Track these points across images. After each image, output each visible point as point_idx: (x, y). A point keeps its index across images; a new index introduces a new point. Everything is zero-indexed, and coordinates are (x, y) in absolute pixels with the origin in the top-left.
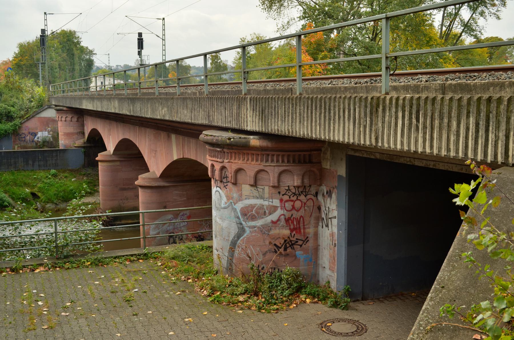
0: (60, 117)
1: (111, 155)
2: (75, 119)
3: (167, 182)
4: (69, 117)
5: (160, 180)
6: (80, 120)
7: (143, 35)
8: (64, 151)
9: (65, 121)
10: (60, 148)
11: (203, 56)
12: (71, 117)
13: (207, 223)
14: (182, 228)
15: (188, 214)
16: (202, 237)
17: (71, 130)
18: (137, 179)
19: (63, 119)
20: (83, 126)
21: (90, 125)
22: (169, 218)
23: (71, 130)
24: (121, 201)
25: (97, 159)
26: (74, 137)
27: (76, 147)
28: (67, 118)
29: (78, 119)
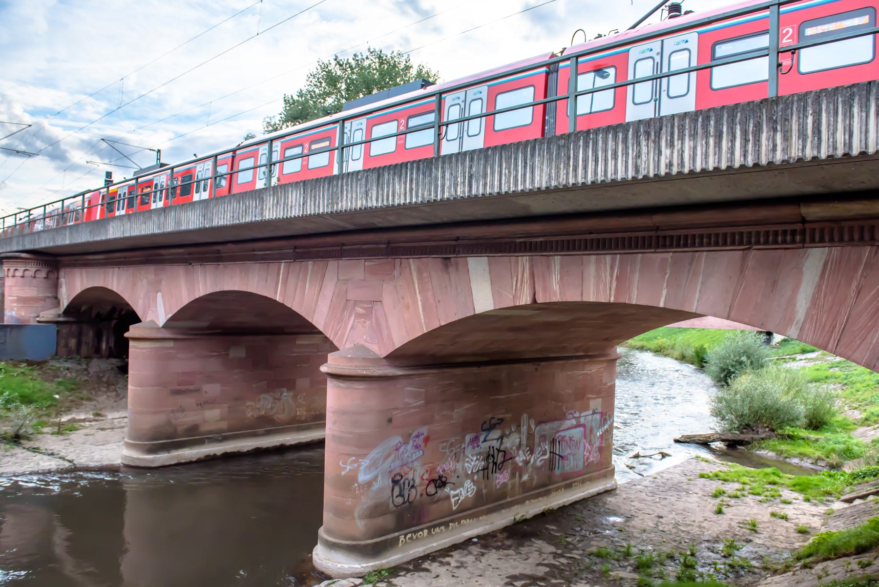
0: (12, 269)
1: (159, 329)
2: (42, 274)
3: (397, 367)
4: (32, 269)
5: (384, 362)
6: (52, 276)
8: (18, 327)
10: (5, 323)
12: (34, 269)
13: (452, 451)
14: (416, 463)
15: (426, 434)
16: (444, 479)
17: (32, 292)
18: (325, 361)
19: (19, 273)
20: (56, 286)
23: (32, 292)
24: (172, 415)
25: (126, 335)
27: (39, 322)
28: (26, 272)
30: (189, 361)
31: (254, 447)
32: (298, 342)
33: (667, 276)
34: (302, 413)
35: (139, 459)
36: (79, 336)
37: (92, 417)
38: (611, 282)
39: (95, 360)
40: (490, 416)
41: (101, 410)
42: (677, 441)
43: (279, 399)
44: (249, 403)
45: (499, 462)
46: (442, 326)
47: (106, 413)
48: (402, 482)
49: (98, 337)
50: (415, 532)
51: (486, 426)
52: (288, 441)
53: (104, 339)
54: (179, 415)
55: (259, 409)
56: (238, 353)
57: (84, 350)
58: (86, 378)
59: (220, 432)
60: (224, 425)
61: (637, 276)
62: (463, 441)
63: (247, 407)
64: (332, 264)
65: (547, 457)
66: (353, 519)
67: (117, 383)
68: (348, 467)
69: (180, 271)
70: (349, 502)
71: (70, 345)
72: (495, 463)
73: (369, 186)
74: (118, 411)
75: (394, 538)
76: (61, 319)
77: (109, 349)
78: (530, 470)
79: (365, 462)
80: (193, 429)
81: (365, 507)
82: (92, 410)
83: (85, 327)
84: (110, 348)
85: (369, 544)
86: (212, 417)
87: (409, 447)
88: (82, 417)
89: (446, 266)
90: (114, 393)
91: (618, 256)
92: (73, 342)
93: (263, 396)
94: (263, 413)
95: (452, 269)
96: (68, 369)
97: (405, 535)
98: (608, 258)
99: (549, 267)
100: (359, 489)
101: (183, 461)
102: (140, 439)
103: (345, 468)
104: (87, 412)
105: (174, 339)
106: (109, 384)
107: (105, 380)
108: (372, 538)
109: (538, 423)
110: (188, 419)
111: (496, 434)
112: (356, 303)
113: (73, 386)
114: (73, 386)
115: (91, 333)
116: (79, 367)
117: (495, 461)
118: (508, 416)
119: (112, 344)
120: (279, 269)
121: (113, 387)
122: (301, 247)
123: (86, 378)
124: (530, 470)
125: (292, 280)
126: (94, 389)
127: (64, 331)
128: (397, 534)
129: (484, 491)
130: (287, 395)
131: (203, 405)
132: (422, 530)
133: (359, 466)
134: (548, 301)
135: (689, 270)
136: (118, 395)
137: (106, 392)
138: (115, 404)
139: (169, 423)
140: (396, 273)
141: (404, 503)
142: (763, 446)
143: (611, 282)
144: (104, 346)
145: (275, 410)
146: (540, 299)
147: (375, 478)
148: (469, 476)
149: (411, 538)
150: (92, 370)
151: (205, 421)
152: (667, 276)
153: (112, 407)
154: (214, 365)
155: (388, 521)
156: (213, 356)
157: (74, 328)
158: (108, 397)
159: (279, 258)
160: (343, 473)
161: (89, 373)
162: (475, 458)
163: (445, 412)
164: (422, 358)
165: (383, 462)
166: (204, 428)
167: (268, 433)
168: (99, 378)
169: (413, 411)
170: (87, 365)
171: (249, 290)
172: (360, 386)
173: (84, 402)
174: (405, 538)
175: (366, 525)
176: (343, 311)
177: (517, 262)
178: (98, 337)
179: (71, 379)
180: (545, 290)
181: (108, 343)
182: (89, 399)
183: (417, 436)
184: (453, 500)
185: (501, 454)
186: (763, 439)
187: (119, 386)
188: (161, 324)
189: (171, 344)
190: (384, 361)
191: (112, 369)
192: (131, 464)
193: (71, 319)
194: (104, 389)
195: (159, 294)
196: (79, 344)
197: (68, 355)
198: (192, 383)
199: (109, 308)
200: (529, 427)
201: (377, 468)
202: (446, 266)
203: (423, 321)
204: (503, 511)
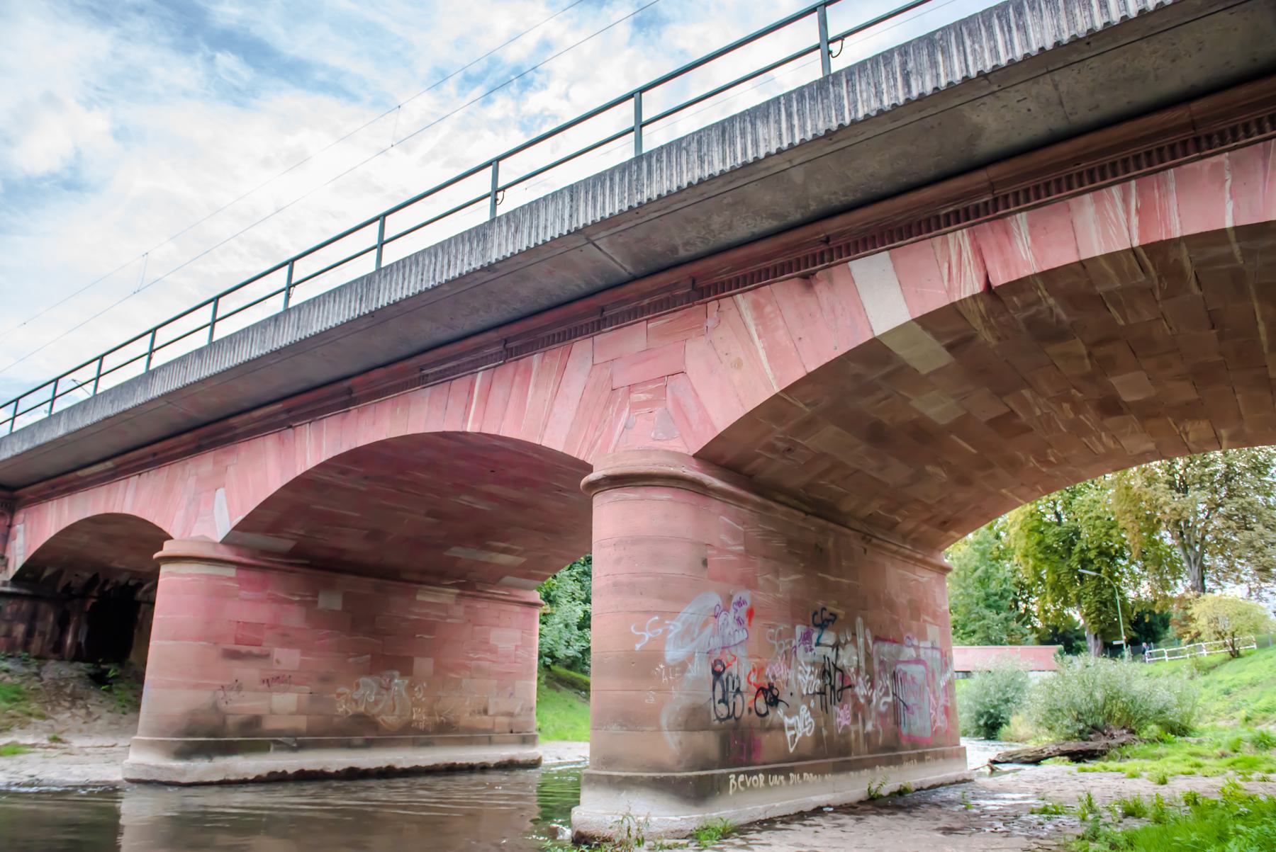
1: (215, 544)
5: (694, 463)
24: (221, 694)
30: (251, 607)
31: (346, 766)
32: (419, 597)
33: (1228, 184)
34: (420, 717)
35: (158, 768)
36: (32, 621)
37: (46, 742)
38: (1128, 220)
39: (52, 662)
40: (820, 604)
41: (62, 732)
42: (971, 781)
43: (388, 689)
44: (341, 690)
45: (837, 688)
46: (809, 375)
47: (69, 739)
48: (724, 676)
49: (62, 624)
50: (750, 774)
51: (818, 620)
52: (399, 761)
53: (71, 629)
54: (233, 695)
55: (356, 701)
56: (331, 601)
57: (36, 644)
58: (38, 685)
59: (295, 734)
60: (301, 723)
61: (1173, 200)
62: (792, 635)
63: (339, 695)
64: (581, 347)
65: (890, 699)
66: (659, 729)
67: (89, 697)
68: (647, 635)
69: (269, 443)
70: (651, 699)
71: (15, 634)
72: (833, 688)
73: (705, 149)
74: (90, 737)
75: (722, 775)
76: (8, 589)
77: (77, 645)
78: (873, 714)
79: (676, 627)
80: (252, 724)
81: (678, 708)
82: (46, 732)
83: (43, 606)
84: (79, 644)
85: (689, 778)
86: (283, 707)
87: (731, 617)
88: (30, 741)
89: (809, 287)
90: (83, 711)
91: (1133, 183)
92: (20, 630)
93: (364, 680)
94: (362, 709)
95: (820, 288)
96: (7, 671)
97: (737, 774)
98: (1115, 190)
99: (1007, 232)
100: (667, 674)
101: (232, 778)
102: (163, 733)
103: (642, 636)
104: (37, 735)
105: (239, 565)
106: (75, 698)
107: (68, 690)
108: (691, 769)
109: (877, 639)
110: (244, 704)
111: (829, 637)
112: (631, 388)
113: (15, 696)
114: (15, 696)
115: (51, 618)
116: (26, 671)
117: (834, 684)
118: (841, 613)
119: (82, 640)
120: (472, 385)
121: (80, 702)
122: (517, 337)
123: (38, 685)
124: (873, 714)
125: (498, 392)
126: (51, 701)
127: (8, 609)
128: (724, 771)
129: (825, 733)
130: (399, 683)
131: (274, 681)
132: (756, 773)
133: (666, 632)
134: (1015, 278)
135: (1265, 166)
136: (89, 714)
137: (69, 709)
138: (84, 727)
139: (215, 707)
140: (710, 323)
141: (729, 717)
142: (1128, 753)
143: (1128, 220)
144: (69, 640)
145: (381, 706)
146: (998, 279)
147: (691, 658)
148: (805, 698)
149: (744, 784)
150: (47, 676)
151: (272, 712)
152: (1228, 184)
153: (80, 731)
154: (294, 618)
155: (708, 742)
156: (291, 602)
157: (25, 606)
158: (73, 716)
159: (472, 368)
160: (638, 646)
161: (42, 680)
162: (809, 669)
163: (768, 576)
164: (739, 466)
165: (701, 632)
166: (270, 724)
167: (369, 744)
168: (59, 688)
169: (731, 557)
170: (39, 667)
171: (409, 432)
172: (662, 496)
173: (33, 720)
174: (736, 780)
175: (680, 743)
176: (606, 407)
177: (947, 242)
178: (62, 624)
179: (12, 685)
180: (1006, 264)
181: (75, 636)
182: (42, 717)
183: (740, 603)
184: (789, 734)
185: (838, 674)
186: (1123, 744)
187: (90, 701)
188: (219, 538)
189: (231, 572)
190: (694, 461)
191: (80, 677)
192: (145, 777)
193: (24, 591)
194: (67, 704)
195: (221, 492)
196: (29, 633)
197: (8, 650)
198: (257, 644)
199: (87, 575)
200: (866, 643)
201: (693, 640)
202: (809, 287)
203: (771, 377)
204: (852, 773)
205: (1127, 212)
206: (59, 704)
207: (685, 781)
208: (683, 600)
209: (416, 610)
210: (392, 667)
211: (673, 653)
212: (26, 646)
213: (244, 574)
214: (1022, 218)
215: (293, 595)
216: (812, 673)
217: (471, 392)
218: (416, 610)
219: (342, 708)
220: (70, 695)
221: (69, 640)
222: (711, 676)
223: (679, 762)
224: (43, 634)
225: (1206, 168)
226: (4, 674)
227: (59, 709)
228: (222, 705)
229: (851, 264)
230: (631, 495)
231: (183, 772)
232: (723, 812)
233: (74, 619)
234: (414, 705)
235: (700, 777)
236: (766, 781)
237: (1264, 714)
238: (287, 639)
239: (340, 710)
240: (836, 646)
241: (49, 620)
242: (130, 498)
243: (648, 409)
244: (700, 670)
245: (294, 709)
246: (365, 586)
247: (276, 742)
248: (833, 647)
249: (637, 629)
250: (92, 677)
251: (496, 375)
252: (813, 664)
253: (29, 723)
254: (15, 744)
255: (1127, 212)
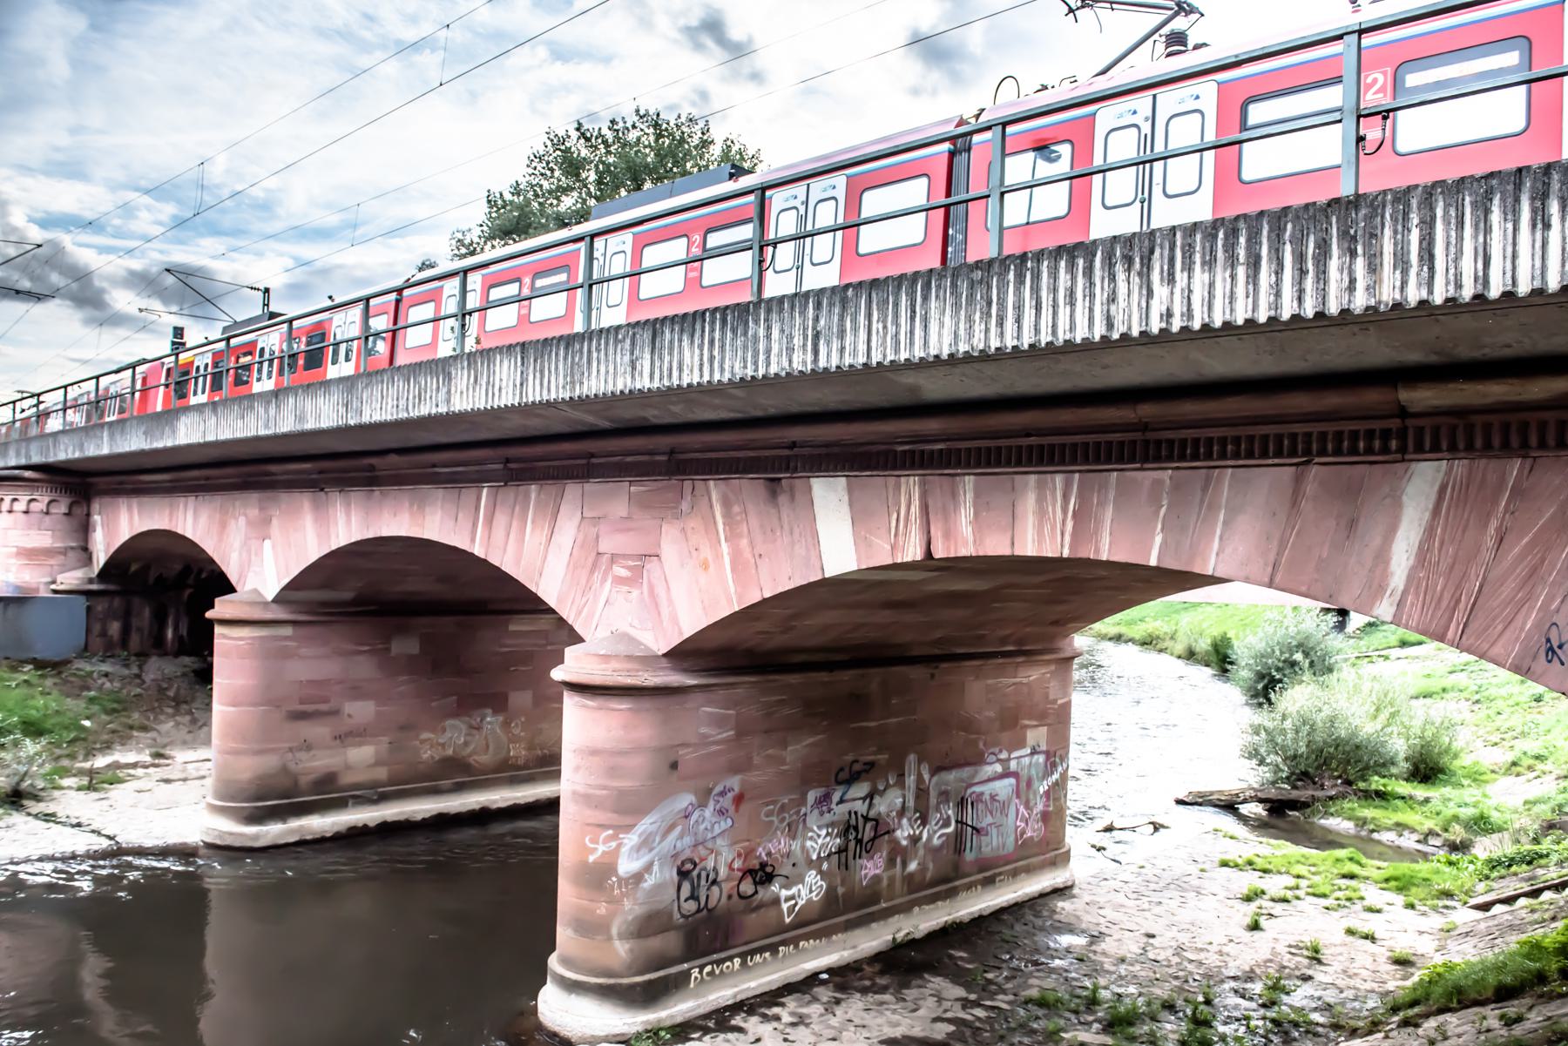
2: (61, 508)
3: (685, 671)
5: (665, 663)
6: (78, 511)
7: (186, 333)
9: (26, 512)
11: (642, 296)
12: (47, 499)
13: (783, 820)
14: (719, 842)
15: (737, 790)
16: (769, 869)
21: (119, 525)
22: (685, 804)
25: (209, 614)
26: (52, 562)
27: (55, 592)
29: (70, 507)
30: (316, 662)
32: (512, 628)
33: (1163, 510)
34: (518, 752)
35: (231, 834)
36: (126, 618)
37: (148, 759)
40: (849, 758)
41: (165, 746)
43: (479, 728)
44: (425, 735)
45: (866, 839)
46: (765, 601)
47: (172, 753)
49: (160, 619)
51: (843, 775)
52: (495, 801)
53: (170, 622)
54: (303, 755)
55: (443, 745)
57: (135, 641)
59: (373, 785)
60: (382, 773)
62: (803, 801)
63: (423, 742)
66: (610, 938)
67: (194, 699)
68: (601, 848)
69: (304, 502)
70: (602, 909)
72: (859, 841)
73: (637, 352)
74: (195, 749)
75: (681, 973)
76: (94, 587)
77: (178, 638)
78: (921, 852)
79: (631, 839)
80: (327, 781)
82: (149, 747)
83: (136, 601)
86: (361, 759)
87: (708, 812)
90: (188, 718)
92: (115, 628)
93: (449, 722)
94: (450, 752)
96: (106, 675)
97: (702, 968)
99: (954, 495)
100: (620, 887)
102: (233, 799)
104: (140, 751)
105: (294, 623)
107: (171, 693)
109: (935, 771)
111: (860, 789)
112: (614, 558)
113: (115, 706)
114: (115, 706)
115: (147, 612)
116: (126, 672)
118: (882, 758)
119: (184, 631)
120: (479, 499)
121: (185, 707)
124: (921, 852)
125: (501, 519)
129: (840, 890)
130: (491, 720)
133: (619, 846)
136: (194, 721)
137: (174, 716)
138: (189, 737)
139: (284, 770)
140: (685, 506)
141: (699, 910)
144: (170, 634)
145: (472, 747)
146: (939, 552)
147: (648, 868)
148: (815, 864)
149: (711, 974)
150: (149, 677)
151: (348, 767)
152: (1163, 510)
154: (364, 668)
155: (670, 942)
157: (117, 602)
158: (178, 724)
159: (478, 479)
162: (824, 832)
166: (347, 779)
167: (459, 788)
168: (162, 690)
170: (140, 667)
174: (701, 972)
176: (592, 571)
178: (160, 619)
180: (947, 535)
181: (176, 629)
182: (144, 729)
184: (785, 906)
186: (1331, 798)
187: (195, 705)
189: (288, 631)
191: (184, 675)
192: (218, 842)
193: (111, 587)
194: (170, 711)
196: (126, 631)
198: (325, 700)
199: (178, 567)
201: (651, 850)
203: (732, 590)
205: (1065, 511)
206: (162, 712)
207: (633, 986)
208: (640, 811)
209: (509, 642)
210: (486, 706)
211: (627, 865)
212: (124, 641)
213: (303, 631)
214: (969, 481)
215: (362, 644)
216: (828, 834)
217: (477, 508)
218: (509, 642)
219: (426, 754)
220: (174, 699)
221: (170, 634)
222: (676, 877)
223: (630, 967)
224: (139, 630)
225: (1147, 483)
226: (104, 679)
227: (162, 717)
228: (292, 766)
229: (813, 480)
230: (590, 703)
231: (256, 837)
232: (679, 1009)
233: (172, 611)
234: (510, 741)
235: (650, 982)
236: (744, 963)
237: (1531, 762)
238: (357, 691)
239: (425, 756)
240: (870, 796)
241: (144, 616)
242: (191, 520)
243: (626, 588)
244: (663, 875)
245: (372, 761)
246: (447, 623)
247: (353, 797)
248: (864, 799)
249: (592, 841)
250: (196, 672)
251: (499, 497)
252: (832, 824)
253: (131, 737)
254: (117, 766)
255: (1065, 511)
